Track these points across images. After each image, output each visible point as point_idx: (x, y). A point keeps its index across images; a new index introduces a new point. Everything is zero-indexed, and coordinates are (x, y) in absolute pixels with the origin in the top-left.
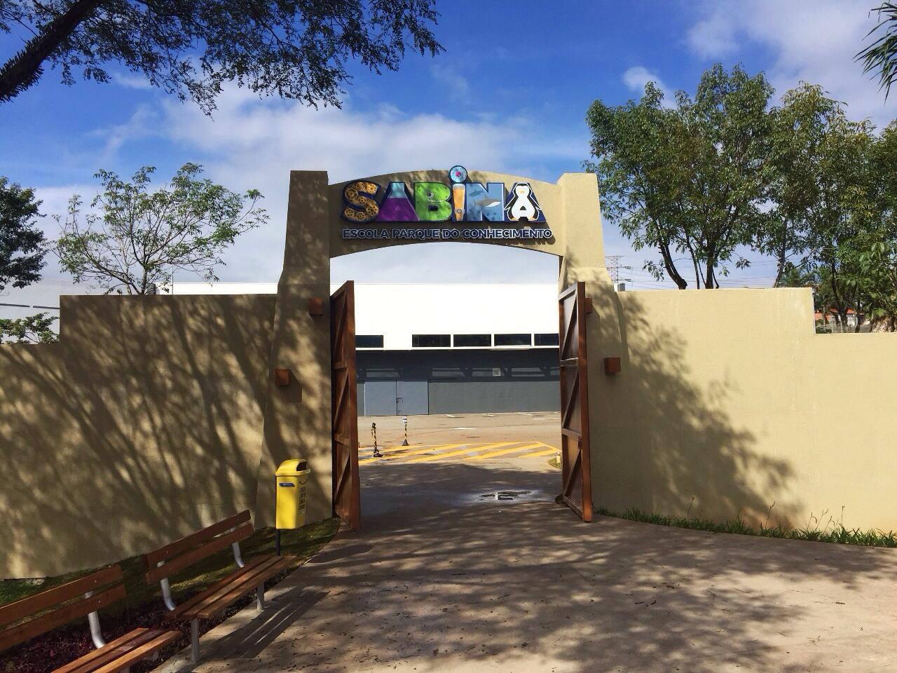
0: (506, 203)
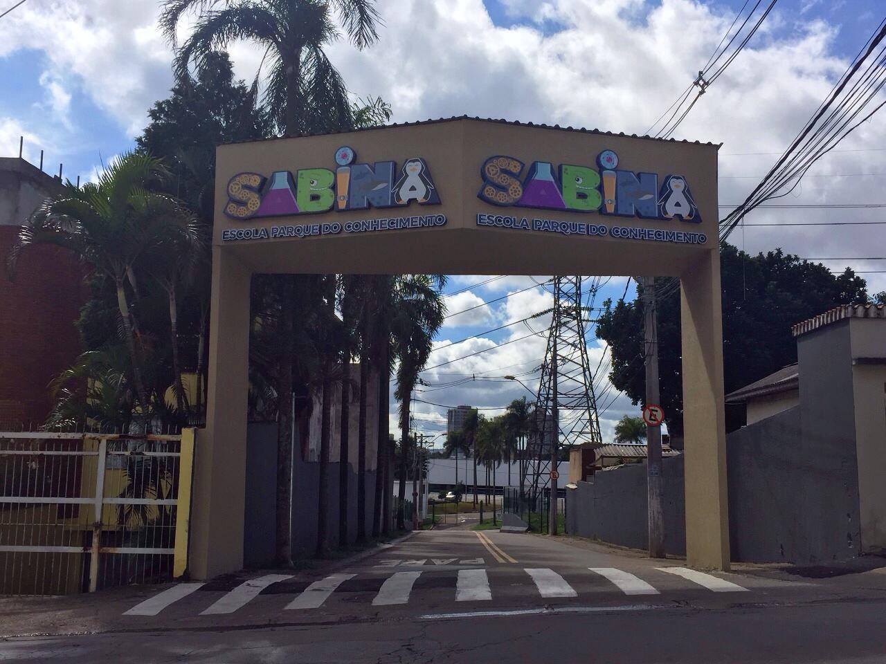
0: (394, 184)
